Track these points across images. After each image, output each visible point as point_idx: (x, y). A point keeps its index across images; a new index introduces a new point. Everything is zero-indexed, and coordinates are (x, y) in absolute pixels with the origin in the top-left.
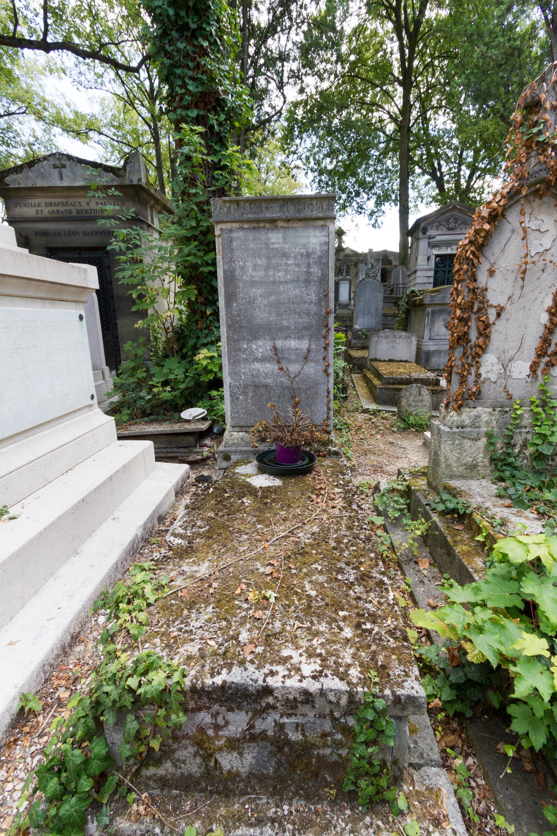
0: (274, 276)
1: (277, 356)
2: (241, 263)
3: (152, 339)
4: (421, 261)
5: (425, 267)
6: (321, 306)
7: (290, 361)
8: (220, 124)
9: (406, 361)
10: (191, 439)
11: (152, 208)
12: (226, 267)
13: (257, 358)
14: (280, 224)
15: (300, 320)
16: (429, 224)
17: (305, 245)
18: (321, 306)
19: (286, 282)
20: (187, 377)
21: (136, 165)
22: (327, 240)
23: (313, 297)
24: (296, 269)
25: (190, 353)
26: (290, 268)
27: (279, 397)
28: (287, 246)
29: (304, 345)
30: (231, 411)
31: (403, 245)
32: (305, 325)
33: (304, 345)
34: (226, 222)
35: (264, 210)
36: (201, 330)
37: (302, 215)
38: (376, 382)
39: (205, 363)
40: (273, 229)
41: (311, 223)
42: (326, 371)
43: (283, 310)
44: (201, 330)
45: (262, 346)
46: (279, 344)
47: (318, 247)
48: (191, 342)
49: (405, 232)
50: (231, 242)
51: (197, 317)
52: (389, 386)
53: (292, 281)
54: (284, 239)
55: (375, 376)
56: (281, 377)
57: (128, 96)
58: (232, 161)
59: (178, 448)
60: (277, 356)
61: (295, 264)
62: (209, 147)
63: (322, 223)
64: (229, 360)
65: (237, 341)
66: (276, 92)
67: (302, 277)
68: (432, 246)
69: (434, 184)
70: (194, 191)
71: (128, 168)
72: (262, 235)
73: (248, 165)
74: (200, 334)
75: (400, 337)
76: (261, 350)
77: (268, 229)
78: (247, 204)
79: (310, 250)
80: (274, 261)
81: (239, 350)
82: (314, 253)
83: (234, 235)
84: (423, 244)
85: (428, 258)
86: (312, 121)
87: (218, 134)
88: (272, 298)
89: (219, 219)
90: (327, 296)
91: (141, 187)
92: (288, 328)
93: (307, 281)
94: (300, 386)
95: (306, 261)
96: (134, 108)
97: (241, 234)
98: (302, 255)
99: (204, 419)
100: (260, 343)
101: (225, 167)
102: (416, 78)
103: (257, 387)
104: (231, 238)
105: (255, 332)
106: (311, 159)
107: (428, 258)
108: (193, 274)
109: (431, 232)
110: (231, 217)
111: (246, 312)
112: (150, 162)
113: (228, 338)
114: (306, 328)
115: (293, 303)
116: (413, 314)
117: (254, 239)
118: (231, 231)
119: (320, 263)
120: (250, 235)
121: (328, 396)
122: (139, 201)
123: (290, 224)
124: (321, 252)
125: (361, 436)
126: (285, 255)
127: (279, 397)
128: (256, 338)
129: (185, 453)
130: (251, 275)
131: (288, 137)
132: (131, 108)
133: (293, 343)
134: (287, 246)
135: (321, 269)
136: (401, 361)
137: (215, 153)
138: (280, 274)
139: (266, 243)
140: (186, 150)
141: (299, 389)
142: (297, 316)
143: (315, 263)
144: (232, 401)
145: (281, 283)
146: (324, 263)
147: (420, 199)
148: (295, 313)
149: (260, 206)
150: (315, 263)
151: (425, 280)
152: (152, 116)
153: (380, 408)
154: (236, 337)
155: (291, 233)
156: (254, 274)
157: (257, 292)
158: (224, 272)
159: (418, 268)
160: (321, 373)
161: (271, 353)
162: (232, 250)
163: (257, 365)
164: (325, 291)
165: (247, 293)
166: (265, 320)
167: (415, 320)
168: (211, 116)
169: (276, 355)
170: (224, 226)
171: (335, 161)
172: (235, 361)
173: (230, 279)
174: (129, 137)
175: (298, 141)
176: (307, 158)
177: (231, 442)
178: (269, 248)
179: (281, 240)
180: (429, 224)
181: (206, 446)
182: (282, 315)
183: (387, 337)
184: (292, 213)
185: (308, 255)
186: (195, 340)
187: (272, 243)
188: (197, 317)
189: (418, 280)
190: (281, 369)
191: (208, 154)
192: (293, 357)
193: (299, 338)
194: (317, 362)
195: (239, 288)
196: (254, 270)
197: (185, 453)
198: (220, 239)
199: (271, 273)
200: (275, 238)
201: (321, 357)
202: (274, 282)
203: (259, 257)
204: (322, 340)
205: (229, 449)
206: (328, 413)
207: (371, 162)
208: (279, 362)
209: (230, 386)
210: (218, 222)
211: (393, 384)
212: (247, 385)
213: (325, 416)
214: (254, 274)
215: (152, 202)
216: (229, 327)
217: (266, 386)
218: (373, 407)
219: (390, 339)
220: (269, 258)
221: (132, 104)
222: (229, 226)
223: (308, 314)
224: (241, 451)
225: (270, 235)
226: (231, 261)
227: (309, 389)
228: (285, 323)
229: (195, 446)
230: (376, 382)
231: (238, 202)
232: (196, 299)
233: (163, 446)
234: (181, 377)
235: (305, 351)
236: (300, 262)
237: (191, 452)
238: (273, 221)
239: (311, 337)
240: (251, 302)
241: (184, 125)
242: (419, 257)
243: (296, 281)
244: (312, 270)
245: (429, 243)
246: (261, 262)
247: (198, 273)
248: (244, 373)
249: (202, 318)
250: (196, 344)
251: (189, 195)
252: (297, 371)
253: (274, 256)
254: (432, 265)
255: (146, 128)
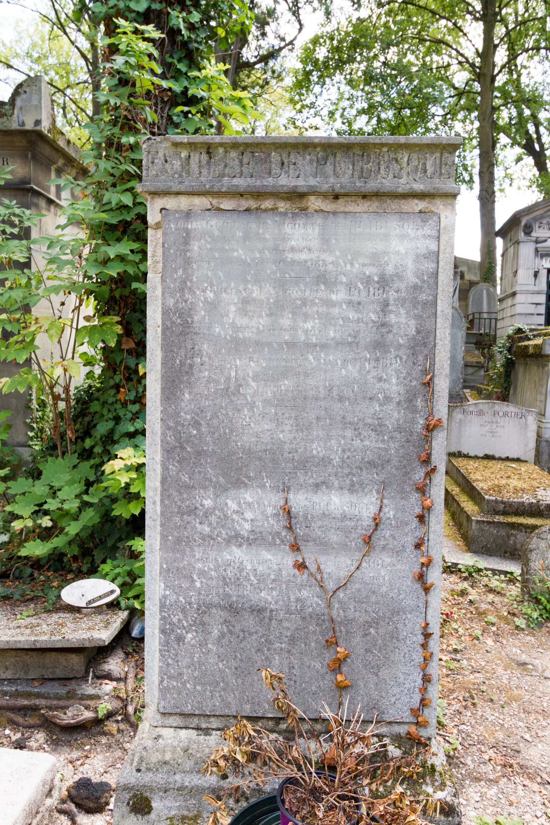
0: (294, 328)
1: (292, 530)
2: (210, 295)
3: (34, 405)
4: (524, 277)
5: (531, 288)
6: (414, 410)
7: (324, 546)
8: (191, 27)
9: (518, 460)
10: (76, 661)
11: (59, 172)
12: (171, 302)
13: (237, 536)
14: (314, 203)
15: (357, 443)
16: (535, 219)
17: (375, 258)
18: (414, 410)
19: (323, 346)
20: (85, 505)
21: (35, 97)
22: (433, 247)
23: (394, 387)
24: (352, 315)
25: (98, 450)
26: (336, 311)
27: (292, 640)
28: (329, 258)
29: (365, 506)
30: (162, 673)
31: (488, 250)
32: (369, 456)
33: (365, 506)
34: (178, 193)
35: (276, 170)
36: (124, 404)
37: (372, 185)
38: (469, 506)
39: (124, 479)
40: (295, 215)
41: (394, 205)
42: (421, 577)
43: (312, 416)
44: (124, 404)
45: (254, 506)
46: (299, 501)
47: (410, 264)
48: (102, 428)
49: (489, 232)
50: (186, 241)
51: (118, 378)
52: (498, 518)
53: (340, 344)
54: (325, 240)
55: (463, 490)
56: (301, 587)
57: (58, 18)
58: (210, 89)
59: (44, 680)
60: (292, 530)
61: (350, 303)
62: (167, 66)
63: (421, 205)
64: (164, 537)
65: (189, 488)
66: (289, 15)
67: (367, 335)
68: (541, 254)
69: (529, 160)
70: (132, 140)
71: (18, 102)
72: (268, 229)
73: (240, 99)
74: (121, 413)
75: (505, 414)
76: (249, 515)
77: (285, 214)
78: (233, 154)
79: (390, 270)
80: (295, 293)
81: (193, 511)
82: (399, 277)
83: (195, 225)
84: (526, 250)
85: (536, 274)
86: (340, 65)
87: (185, 44)
88: (286, 384)
89: (160, 186)
90: (429, 384)
91: (40, 135)
92: (325, 461)
93: (380, 346)
94: (351, 614)
95: (380, 296)
96: (65, 33)
97: (213, 224)
98: (368, 281)
99: (114, 605)
100: (248, 496)
101: (193, 101)
102: (501, 9)
103: (236, 613)
104: (188, 232)
105: (235, 471)
106: (338, 115)
107: (536, 274)
108: (117, 294)
109: (539, 233)
110: (188, 184)
111: (215, 415)
112: (83, 110)
113: (164, 481)
114: (372, 464)
115: (341, 399)
116: (520, 370)
117: (246, 237)
118: (188, 214)
119: (415, 302)
120: (238, 227)
121: (424, 646)
122: (34, 158)
123: (340, 205)
124: (419, 275)
125: (454, 643)
126: (323, 279)
127: (292, 640)
128: (238, 484)
129: (59, 698)
130: (233, 325)
131: (303, 83)
132: (60, 33)
133: (336, 502)
134: (329, 258)
135: (417, 317)
136: (507, 459)
137: (177, 75)
138: (309, 325)
139: (276, 249)
140: (119, 61)
141: (349, 622)
142: (349, 433)
143: (402, 302)
144: (165, 646)
145: (310, 346)
146: (425, 304)
147: (508, 181)
148: (345, 423)
149: (267, 160)
150: (402, 302)
151: (532, 309)
152: (92, 45)
153: (482, 563)
154: (185, 478)
155: (341, 228)
156: (242, 321)
157: (246, 366)
158: (165, 313)
159: (517, 288)
160: (409, 584)
161: (277, 525)
162: (188, 262)
163: (238, 554)
164: (425, 372)
165: (222, 368)
166: (266, 438)
167: (524, 378)
168: (174, 13)
169: (290, 528)
170: (170, 203)
171: (374, 121)
172: (178, 541)
173: (180, 329)
174: (52, 73)
175: (317, 89)
176: (332, 114)
177: (155, 758)
178: (284, 261)
179: (315, 243)
180: (535, 219)
181: (109, 677)
182: (309, 427)
183: (481, 413)
184: (345, 180)
185: (384, 282)
186: (111, 424)
187: (293, 249)
188: (118, 378)
189: (519, 309)
190: (301, 566)
191: (163, 76)
192: (334, 537)
193: (352, 489)
194: (398, 552)
195: (200, 354)
196: (243, 312)
197: (59, 698)
198: (160, 233)
199: (286, 321)
200: (301, 236)
201: (410, 540)
202: (291, 345)
203: (257, 281)
204: (415, 496)
205: (147, 778)
206: (424, 690)
207: (431, 125)
208: (295, 548)
209: (162, 606)
210: (155, 194)
211: (505, 513)
212: (210, 606)
213: (417, 697)
214: (242, 321)
215: (61, 162)
216: (168, 452)
217: (258, 610)
218: (467, 560)
219: (488, 417)
220: (282, 284)
221: (62, 28)
222: (184, 202)
223: (378, 428)
224: (181, 789)
225: (288, 229)
226: (184, 286)
227: (375, 623)
228: (317, 449)
229: (84, 678)
230: (469, 506)
231: (209, 149)
232: (119, 343)
233: (9, 675)
234: (73, 505)
235: (368, 522)
236: (363, 297)
237: (71, 696)
238: (296, 196)
239: (384, 487)
240: (231, 391)
241: (121, 22)
242: (520, 272)
243: (351, 343)
244: (392, 318)
245: (537, 250)
246: (263, 293)
247: (126, 292)
248: (202, 573)
249: (129, 379)
250: (112, 432)
251: (119, 148)
252: (343, 574)
253: (297, 280)
254: (542, 284)
255: (83, 62)
